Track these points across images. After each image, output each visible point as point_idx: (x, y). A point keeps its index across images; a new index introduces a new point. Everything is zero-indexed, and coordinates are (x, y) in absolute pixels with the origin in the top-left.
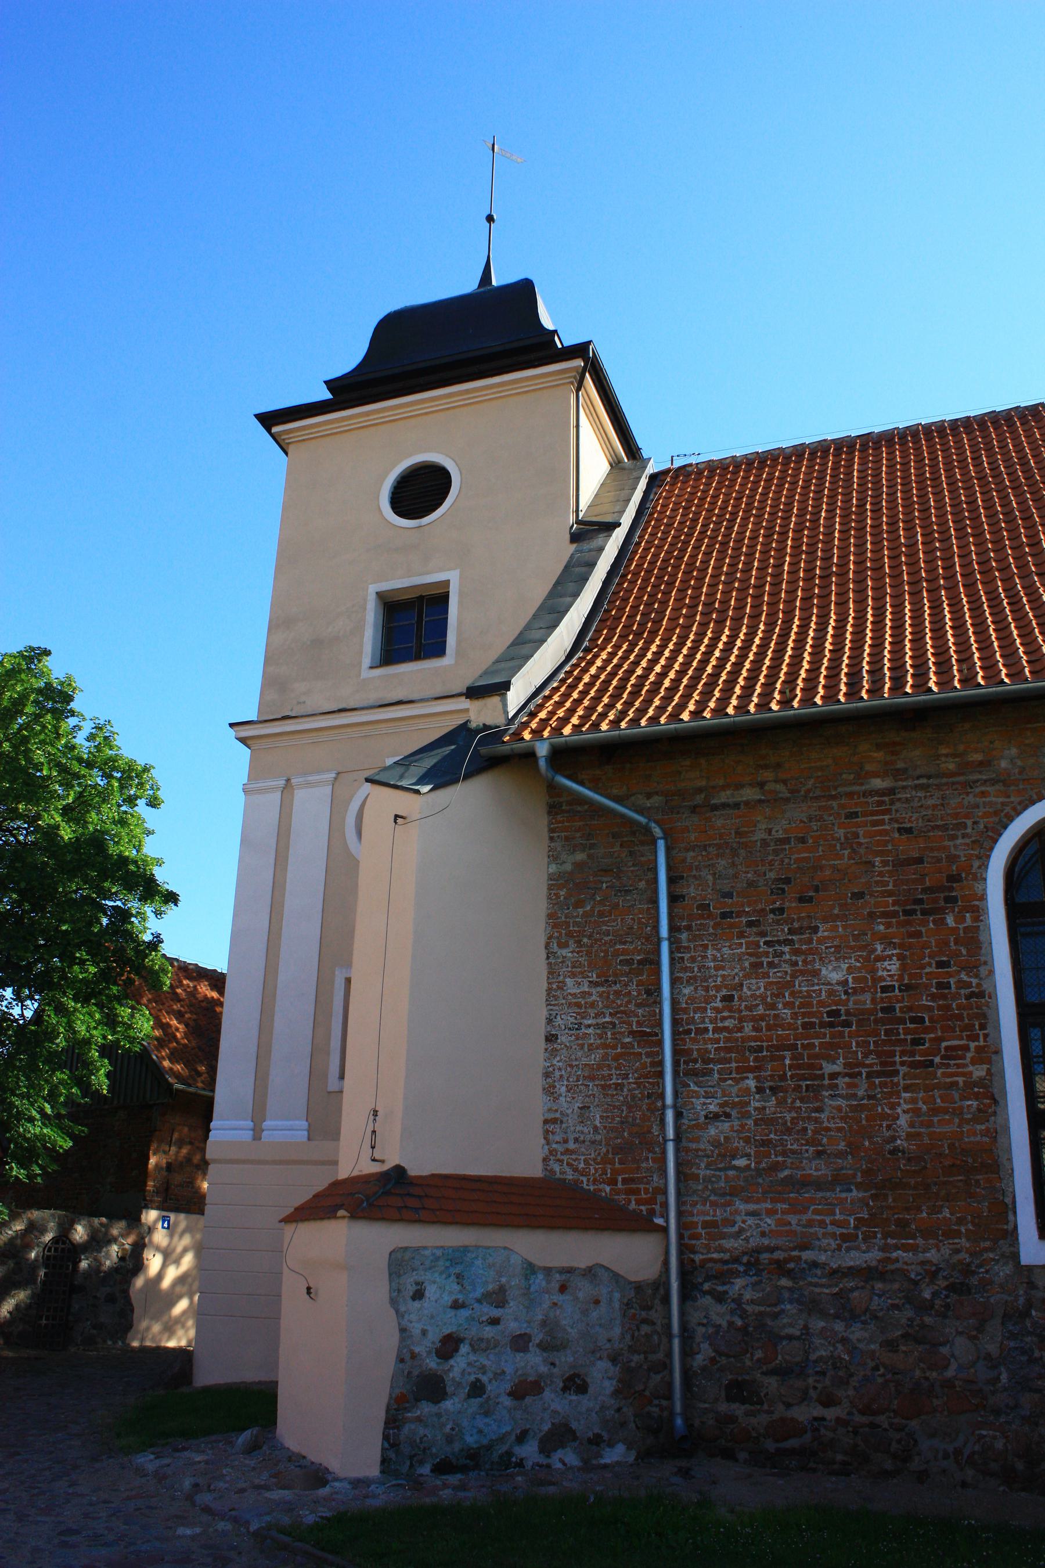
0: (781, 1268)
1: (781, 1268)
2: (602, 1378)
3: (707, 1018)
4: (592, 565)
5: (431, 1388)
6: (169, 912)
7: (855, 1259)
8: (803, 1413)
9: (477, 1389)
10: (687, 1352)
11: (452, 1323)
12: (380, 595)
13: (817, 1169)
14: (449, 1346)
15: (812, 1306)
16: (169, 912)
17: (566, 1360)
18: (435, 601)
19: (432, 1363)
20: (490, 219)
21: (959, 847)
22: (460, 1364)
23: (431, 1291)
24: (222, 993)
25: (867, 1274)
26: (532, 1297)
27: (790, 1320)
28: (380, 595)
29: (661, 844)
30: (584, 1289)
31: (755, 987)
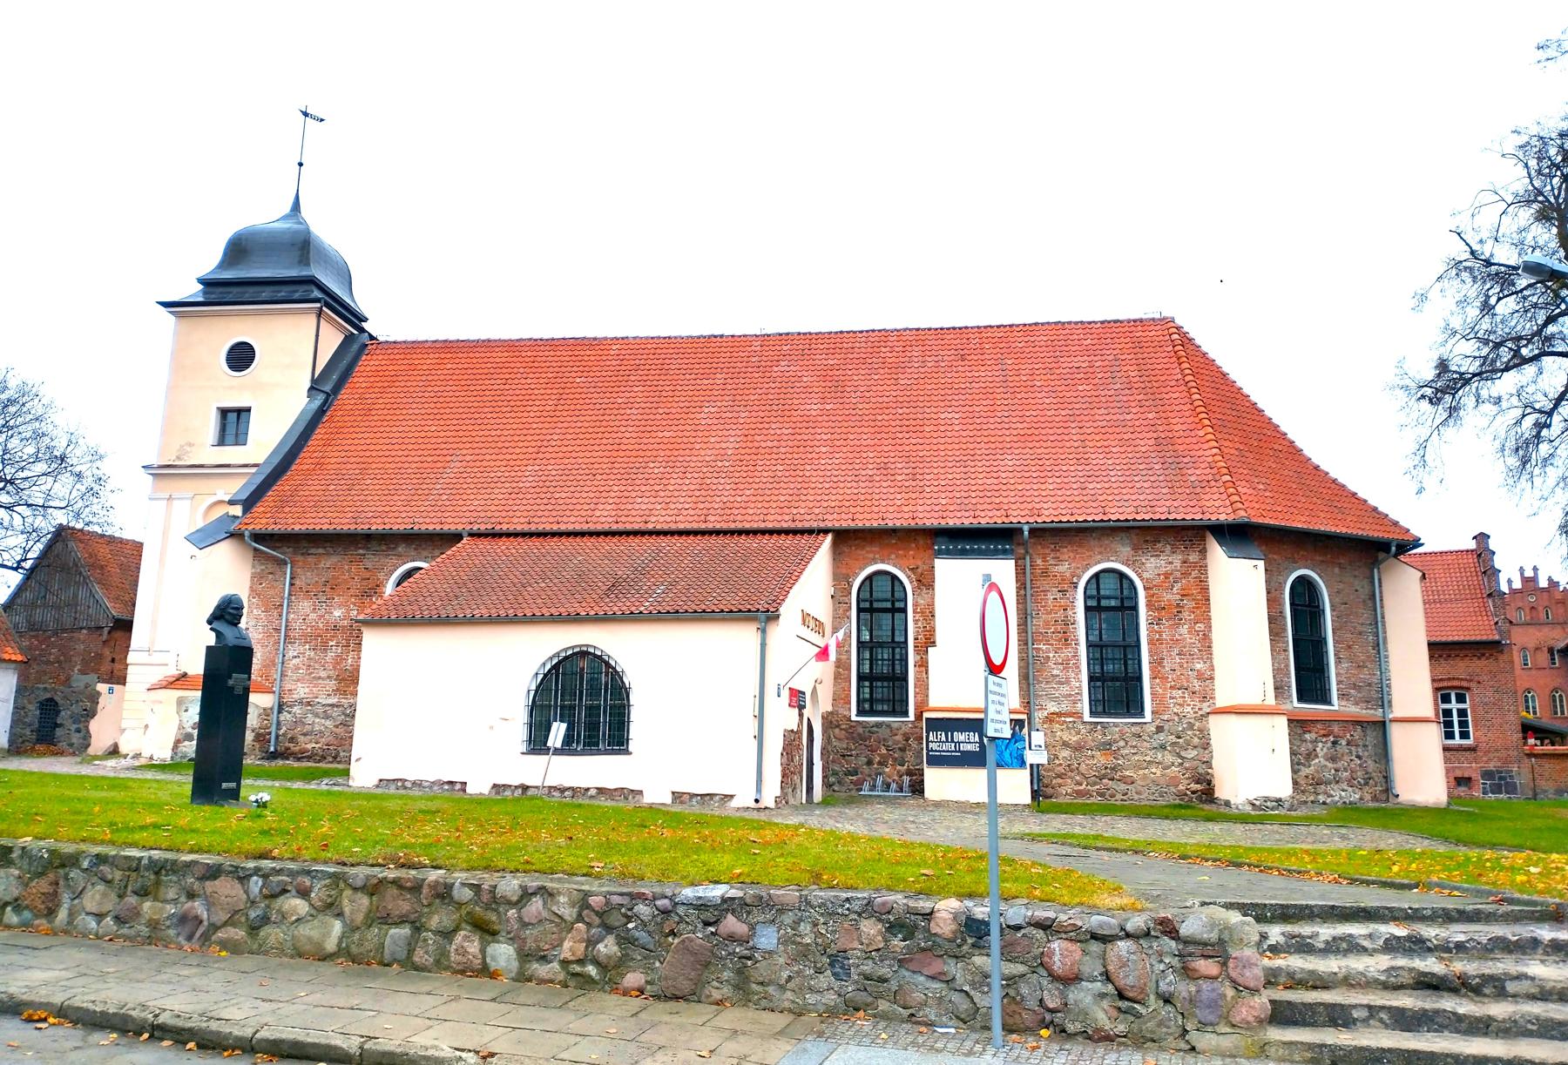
0: (309, 704)
1: (309, 704)
3: (296, 625)
7: (330, 701)
8: (309, 746)
10: (278, 728)
13: (323, 674)
15: (317, 715)
18: (242, 413)
21: (381, 576)
24: (557, 752)
25: (332, 705)
26: (77, 469)
27: (310, 719)
31: (313, 616)
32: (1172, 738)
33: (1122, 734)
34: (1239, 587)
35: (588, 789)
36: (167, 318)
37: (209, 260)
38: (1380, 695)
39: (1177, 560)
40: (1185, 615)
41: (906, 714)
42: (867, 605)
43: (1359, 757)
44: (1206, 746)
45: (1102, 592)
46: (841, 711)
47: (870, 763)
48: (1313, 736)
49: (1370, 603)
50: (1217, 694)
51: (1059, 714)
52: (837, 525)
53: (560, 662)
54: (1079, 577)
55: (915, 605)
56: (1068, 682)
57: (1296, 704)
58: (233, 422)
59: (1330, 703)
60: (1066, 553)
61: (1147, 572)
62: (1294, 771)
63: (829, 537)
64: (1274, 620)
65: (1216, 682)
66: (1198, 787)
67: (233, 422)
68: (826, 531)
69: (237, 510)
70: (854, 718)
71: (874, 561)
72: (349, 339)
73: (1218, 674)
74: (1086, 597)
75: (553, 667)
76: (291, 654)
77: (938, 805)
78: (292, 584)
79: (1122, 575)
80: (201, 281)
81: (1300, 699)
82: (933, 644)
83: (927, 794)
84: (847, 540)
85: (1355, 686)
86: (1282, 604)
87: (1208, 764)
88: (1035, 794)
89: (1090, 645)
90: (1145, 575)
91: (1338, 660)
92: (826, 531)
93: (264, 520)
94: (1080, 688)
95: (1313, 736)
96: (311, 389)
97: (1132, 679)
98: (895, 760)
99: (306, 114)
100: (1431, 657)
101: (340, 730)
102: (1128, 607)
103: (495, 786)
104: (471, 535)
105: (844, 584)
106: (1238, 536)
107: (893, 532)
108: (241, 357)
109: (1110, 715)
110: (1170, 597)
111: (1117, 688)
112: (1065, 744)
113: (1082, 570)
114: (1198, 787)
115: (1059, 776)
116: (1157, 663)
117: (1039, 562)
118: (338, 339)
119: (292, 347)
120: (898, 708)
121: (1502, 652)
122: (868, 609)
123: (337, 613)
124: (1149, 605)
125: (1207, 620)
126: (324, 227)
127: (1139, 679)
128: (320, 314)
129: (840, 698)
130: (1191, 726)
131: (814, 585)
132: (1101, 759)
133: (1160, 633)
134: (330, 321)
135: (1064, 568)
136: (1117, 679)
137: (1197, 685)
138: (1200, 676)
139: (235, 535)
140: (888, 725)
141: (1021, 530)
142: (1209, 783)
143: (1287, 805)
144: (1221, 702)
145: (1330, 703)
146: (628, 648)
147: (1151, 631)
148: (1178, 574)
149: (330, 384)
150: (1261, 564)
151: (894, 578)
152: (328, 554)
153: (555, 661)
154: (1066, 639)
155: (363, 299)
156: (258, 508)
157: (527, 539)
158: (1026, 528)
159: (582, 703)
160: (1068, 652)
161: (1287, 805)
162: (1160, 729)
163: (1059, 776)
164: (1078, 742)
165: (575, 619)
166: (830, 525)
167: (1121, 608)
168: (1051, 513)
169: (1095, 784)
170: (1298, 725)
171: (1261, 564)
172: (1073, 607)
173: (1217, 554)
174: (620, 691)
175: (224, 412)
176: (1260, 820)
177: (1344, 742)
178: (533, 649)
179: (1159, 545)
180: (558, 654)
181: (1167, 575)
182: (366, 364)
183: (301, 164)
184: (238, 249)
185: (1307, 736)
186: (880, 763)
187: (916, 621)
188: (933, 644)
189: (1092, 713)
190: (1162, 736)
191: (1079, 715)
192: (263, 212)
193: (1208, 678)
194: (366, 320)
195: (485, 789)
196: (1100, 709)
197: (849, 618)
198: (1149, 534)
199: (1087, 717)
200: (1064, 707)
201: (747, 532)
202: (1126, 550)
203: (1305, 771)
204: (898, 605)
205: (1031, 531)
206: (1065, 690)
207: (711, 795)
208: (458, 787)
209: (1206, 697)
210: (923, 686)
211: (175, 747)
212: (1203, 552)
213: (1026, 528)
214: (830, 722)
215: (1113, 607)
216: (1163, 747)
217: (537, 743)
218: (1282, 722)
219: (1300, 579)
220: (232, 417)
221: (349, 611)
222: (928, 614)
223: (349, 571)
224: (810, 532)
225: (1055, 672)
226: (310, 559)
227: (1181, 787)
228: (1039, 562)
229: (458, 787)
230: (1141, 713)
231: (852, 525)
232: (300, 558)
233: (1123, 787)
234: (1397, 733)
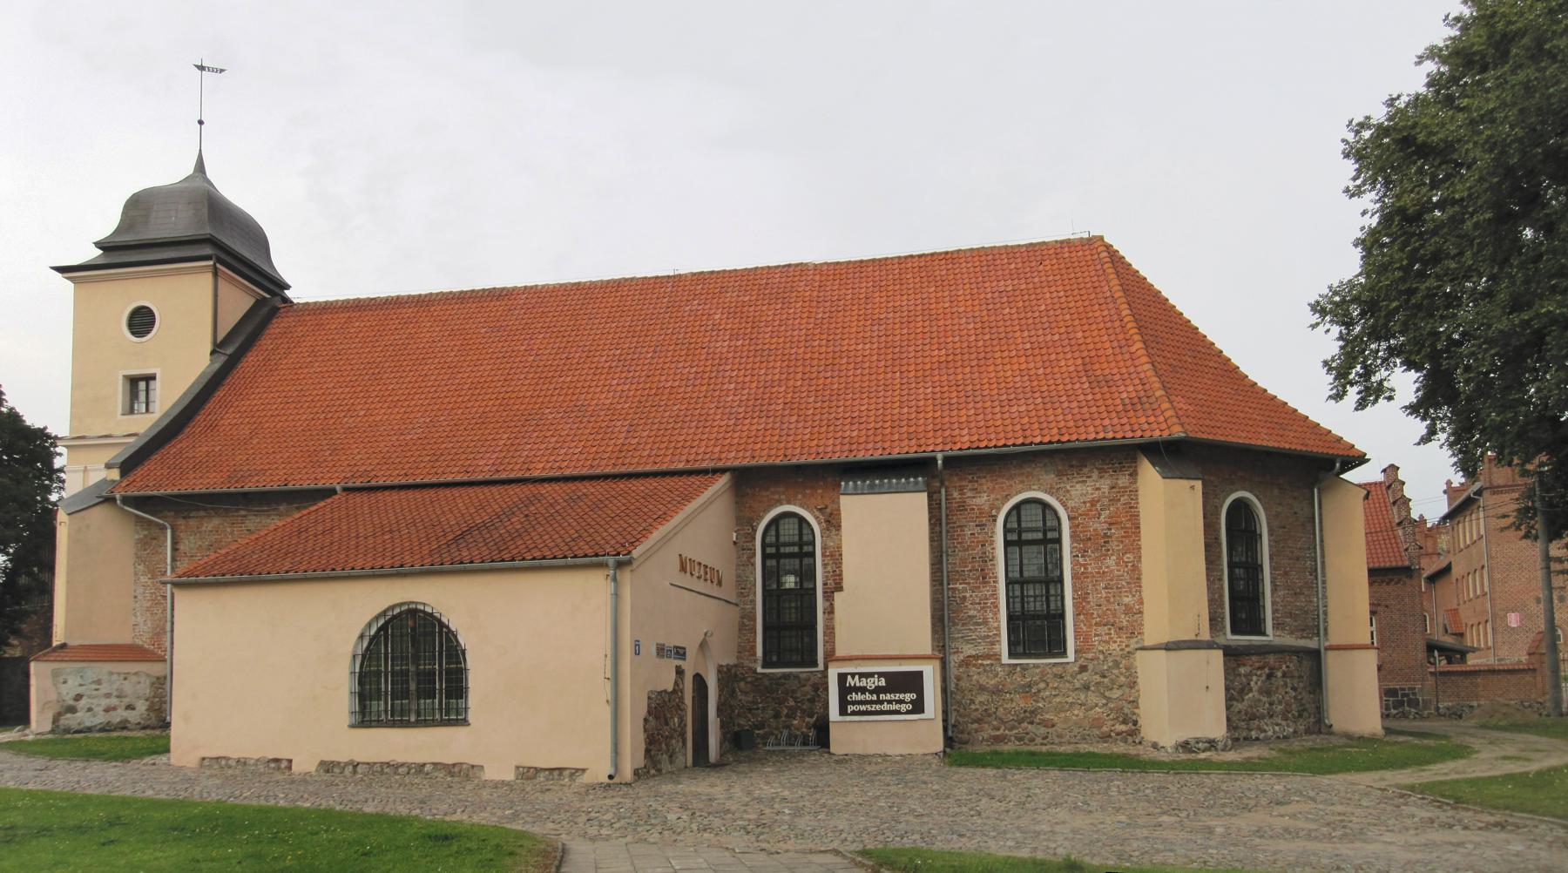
2: (142, 707)
4: (1074, 586)
5: (72, 710)
6: (1326, 291)
9: (90, 710)
11: (80, 690)
12: (125, 377)
14: (78, 697)
16: (1326, 291)
17: (126, 701)
19: (71, 702)
20: (201, 122)
22: (83, 703)
23: (70, 682)
28: (125, 377)
29: (169, 532)
30: (134, 679)
32: (1097, 678)
33: (1043, 674)
34: (1169, 510)
36: (65, 286)
37: (107, 223)
38: (1313, 623)
39: (1105, 484)
40: (1113, 544)
41: (815, 664)
42: (1014, 537)
43: (1294, 689)
44: (1133, 684)
45: (782, 539)
46: (746, 663)
47: (777, 716)
48: (1248, 669)
49: (1309, 527)
50: (1146, 629)
51: (977, 657)
52: (736, 463)
53: (386, 623)
54: (999, 510)
55: (824, 548)
56: (985, 622)
57: (1230, 636)
58: (138, 385)
59: (1264, 634)
60: (986, 484)
61: (1069, 498)
62: (1228, 708)
63: (723, 481)
64: (1211, 546)
65: (1146, 616)
66: (1123, 728)
67: (138, 385)
68: (723, 471)
69: (115, 475)
70: (759, 670)
71: (780, 502)
72: (260, 303)
73: (1146, 608)
74: (1006, 531)
75: (379, 630)
77: (844, 760)
78: (175, 549)
79: (1045, 506)
80: (98, 245)
81: (1234, 632)
82: (840, 589)
83: (832, 750)
84: (750, 482)
85: (1290, 615)
86: (1218, 530)
87: (1135, 703)
88: (949, 741)
89: (1009, 582)
90: (1071, 504)
91: (1275, 589)
92: (723, 471)
93: (155, 480)
94: (998, 629)
95: (1248, 669)
96: (212, 353)
97: (1054, 616)
98: (803, 711)
99: (201, 68)
100: (1371, 584)
102: (1051, 541)
103: (322, 763)
104: (333, 492)
105: (748, 529)
106: (1174, 455)
107: (799, 469)
108: (141, 321)
109: (1029, 656)
110: (1097, 526)
111: (1037, 630)
112: (982, 688)
113: (995, 504)
114: (1123, 728)
115: (978, 721)
117: (956, 494)
118: (246, 303)
119: (191, 308)
121: (1411, 577)
122: (774, 555)
124: (1074, 536)
125: (1137, 550)
126: (237, 189)
127: (1062, 616)
128: (216, 274)
129: (746, 649)
130: (1117, 664)
131: (702, 525)
132: (1020, 703)
133: (1085, 566)
134: (231, 280)
135: (982, 500)
136: (1038, 617)
137: (1124, 620)
138: (1128, 610)
139: (109, 500)
140: (796, 677)
141: (934, 459)
142: (1135, 723)
143: (1220, 746)
144: (1147, 643)
145: (1264, 634)
146: (454, 601)
147: (1075, 563)
148: (1106, 501)
149: (236, 347)
150: (1198, 484)
151: (802, 520)
152: (210, 517)
153: (381, 622)
154: (985, 577)
155: (284, 262)
156: (139, 472)
158: (940, 456)
159: (412, 671)
160: (987, 591)
161: (1220, 746)
162: (1083, 669)
163: (978, 721)
164: (996, 686)
165: (399, 572)
166: (729, 464)
167: (1044, 541)
168: (965, 441)
169: (1013, 728)
170: (1232, 654)
171: (1198, 484)
172: (992, 543)
173: (1148, 473)
174: (455, 654)
175: (133, 381)
176: (1195, 767)
177: (1279, 674)
178: (354, 608)
179: (1085, 470)
180: (384, 613)
181: (1093, 503)
182: (276, 327)
184: (138, 206)
185: (1242, 670)
186: (787, 716)
187: (825, 565)
188: (840, 589)
189: (1011, 655)
190: (1085, 676)
191: (997, 657)
192: (167, 169)
194: (288, 287)
196: (1020, 649)
197: (753, 565)
198: (1072, 458)
199: (1005, 659)
200: (982, 649)
201: (637, 475)
202: (1050, 478)
203: (1238, 706)
204: (806, 549)
205: (946, 460)
206: (983, 631)
207: (561, 770)
208: (284, 764)
209: (1134, 631)
210: (830, 631)
211: (56, 720)
212: (1134, 474)
213: (940, 456)
214: (728, 677)
216: (1086, 688)
217: (364, 718)
218: (1218, 656)
220: (142, 385)
222: (835, 557)
223: (232, 533)
224: (705, 472)
225: (972, 613)
226: (192, 522)
227: (1105, 729)
228: (956, 494)
229: (284, 764)
230: (1064, 654)
231: (753, 463)
232: (181, 522)
233: (1043, 730)
234: (1332, 661)
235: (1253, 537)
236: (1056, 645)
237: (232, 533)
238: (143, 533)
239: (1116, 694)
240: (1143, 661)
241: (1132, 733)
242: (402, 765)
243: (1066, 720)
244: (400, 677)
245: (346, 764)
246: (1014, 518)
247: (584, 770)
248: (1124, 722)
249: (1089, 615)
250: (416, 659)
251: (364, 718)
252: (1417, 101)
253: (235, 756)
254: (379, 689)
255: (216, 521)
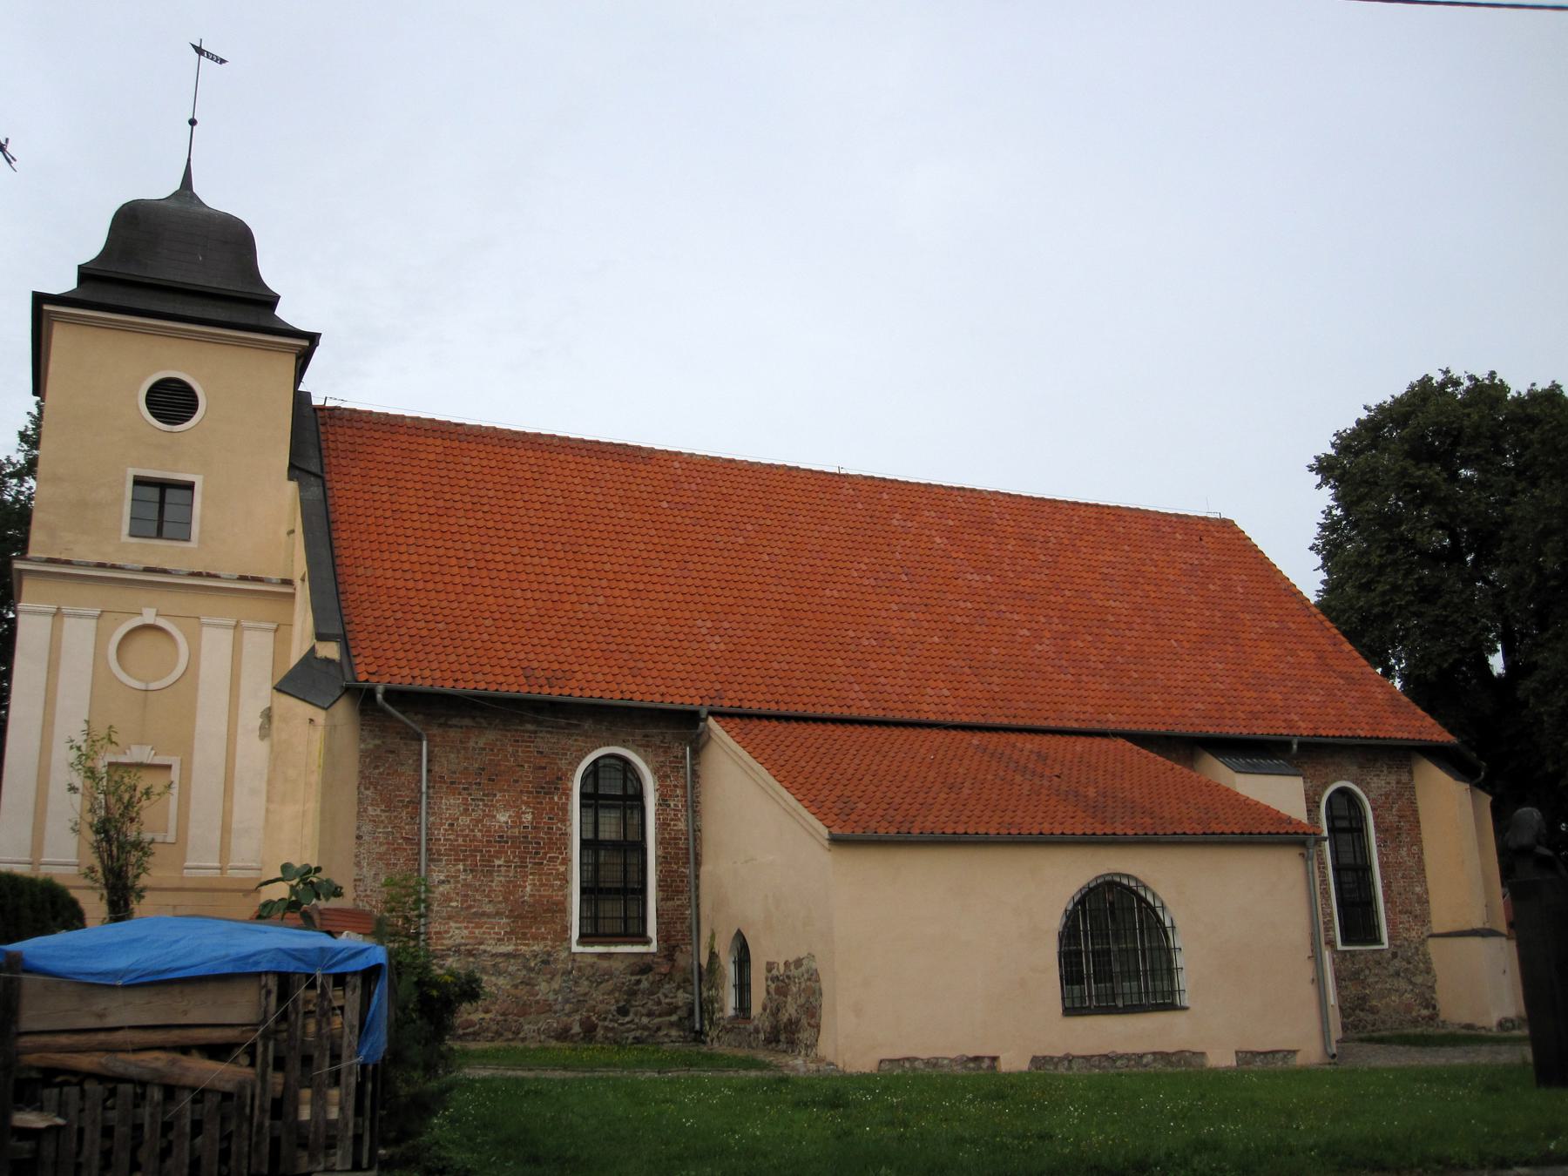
0: (470, 953)
1: (470, 953)
13: (489, 908)
21: (563, 764)
25: (507, 955)
31: (464, 820)
35: (1141, 1056)
39: (1393, 778)
42: (1344, 824)
44: (1428, 971)
66: (1425, 1012)
71: (624, 744)
76: (437, 876)
87: (1432, 988)
90: (1372, 795)
99: (200, 51)
101: (522, 991)
114: (1425, 1012)
116: (1387, 887)
120: (633, 929)
123: (503, 817)
124: (1377, 826)
142: (1434, 1007)
144: (1435, 931)
146: (1163, 875)
157: (1033, 736)
159: (1112, 950)
162: (1395, 955)
178: (1062, 878)
181: (1387, 795)
183: (193, 122)
189: (1345, 941)
190: (1397, 963)
193: (1424, 901)
195: (1023, 1065)
202: (1354, 769)
205: (1300, 745)
207: (1274, 1052)
209: (1424, 919)
215: (613, 794)
217: (1073, 1009)
219: (1342, 792)
221: (519, 815)
226: (454, 734)
232: (435, 731)
233: (1370, 1017)
235: (1359, 830)
236: (1372, 936)
237: (514, 754)
238: (373, 743)
239: (1419, 980)
240: (1433, 946)
241: (1432, 1018)
242: (1122, 1057)
243: (1388, 1006)
244: (1101, 957)
245: (1061, 1059)
246: (590, 781)
247: (1295, 1052)
248: (1427, 1007)
249: (1394, 903)
250: (1117, 940)
251: (1073, 1009)
252: (1353, 430)
253: (925, 1055)
254: (1138, 970)
255: (490, 736)
